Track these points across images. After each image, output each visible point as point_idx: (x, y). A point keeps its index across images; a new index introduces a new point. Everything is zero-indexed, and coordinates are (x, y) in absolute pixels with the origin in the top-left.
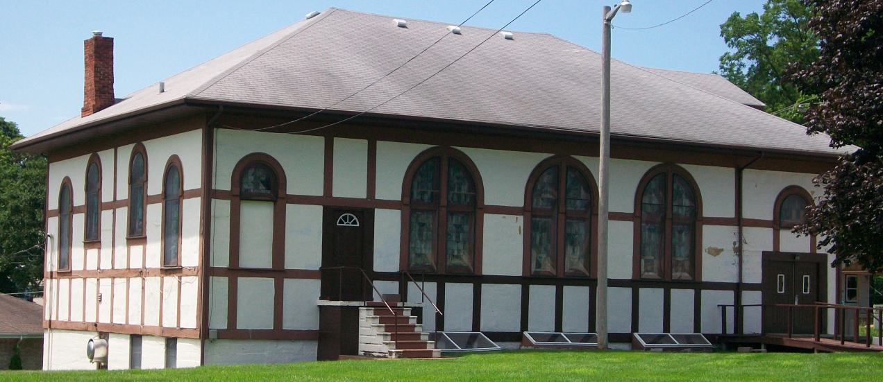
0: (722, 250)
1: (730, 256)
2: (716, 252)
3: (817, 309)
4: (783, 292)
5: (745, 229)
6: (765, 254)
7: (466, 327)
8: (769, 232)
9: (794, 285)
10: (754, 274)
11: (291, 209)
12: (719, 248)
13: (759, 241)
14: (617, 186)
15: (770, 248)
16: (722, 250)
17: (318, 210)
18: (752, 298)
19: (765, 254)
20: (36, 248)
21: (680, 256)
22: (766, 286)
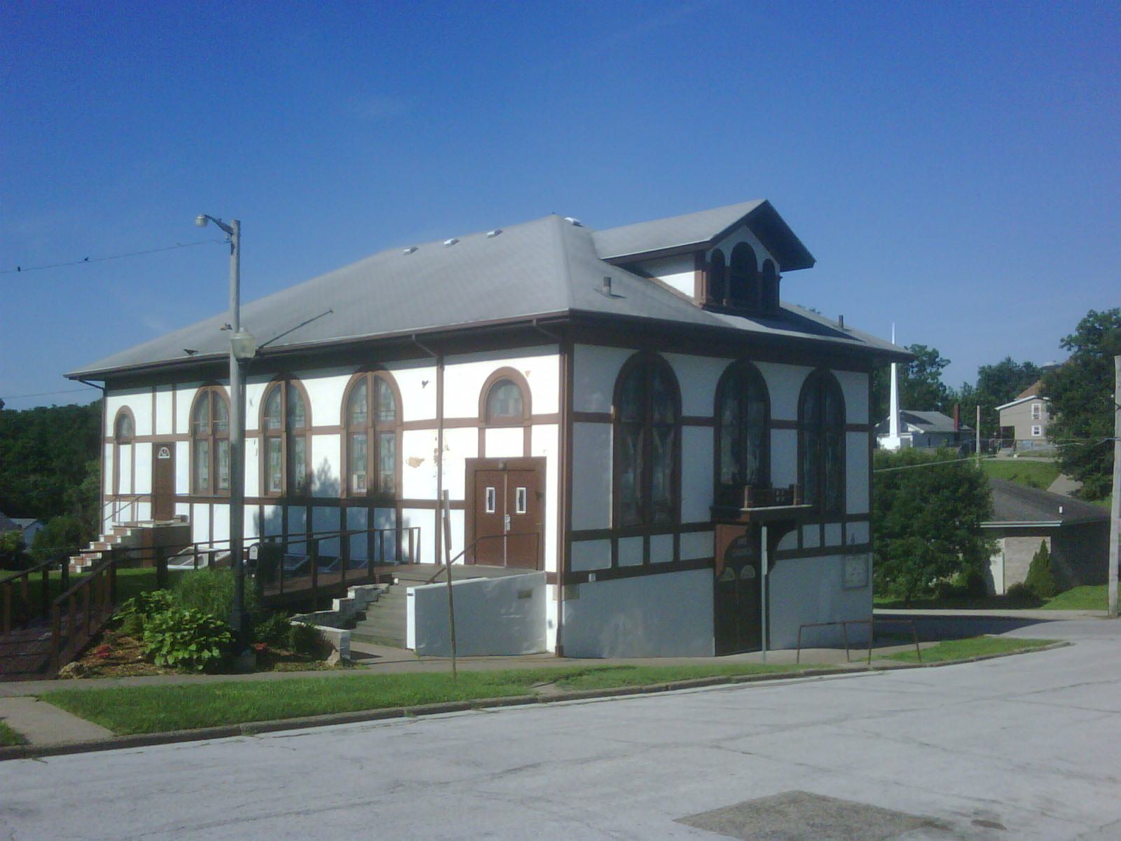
0: (423, 460)
1: (430, 466)
2: (416, 462)
3: (795, 502)
4: (524, 512)
5: (446, 432)
6: (469, 462)
7: (208, 545)
8: (536, 429)
9: (505, 502)
10: (457, 491)
11: (475, 431)
12: (420, 458)
13: (463, 445)
14: (784, 389)
15: (474, 454)
16: (423, 460)
17: (490, 433)
18: (458, 519)
19: (469, 462)
20: (885, 430)
21: (389, 470)
22: (472, 505)
